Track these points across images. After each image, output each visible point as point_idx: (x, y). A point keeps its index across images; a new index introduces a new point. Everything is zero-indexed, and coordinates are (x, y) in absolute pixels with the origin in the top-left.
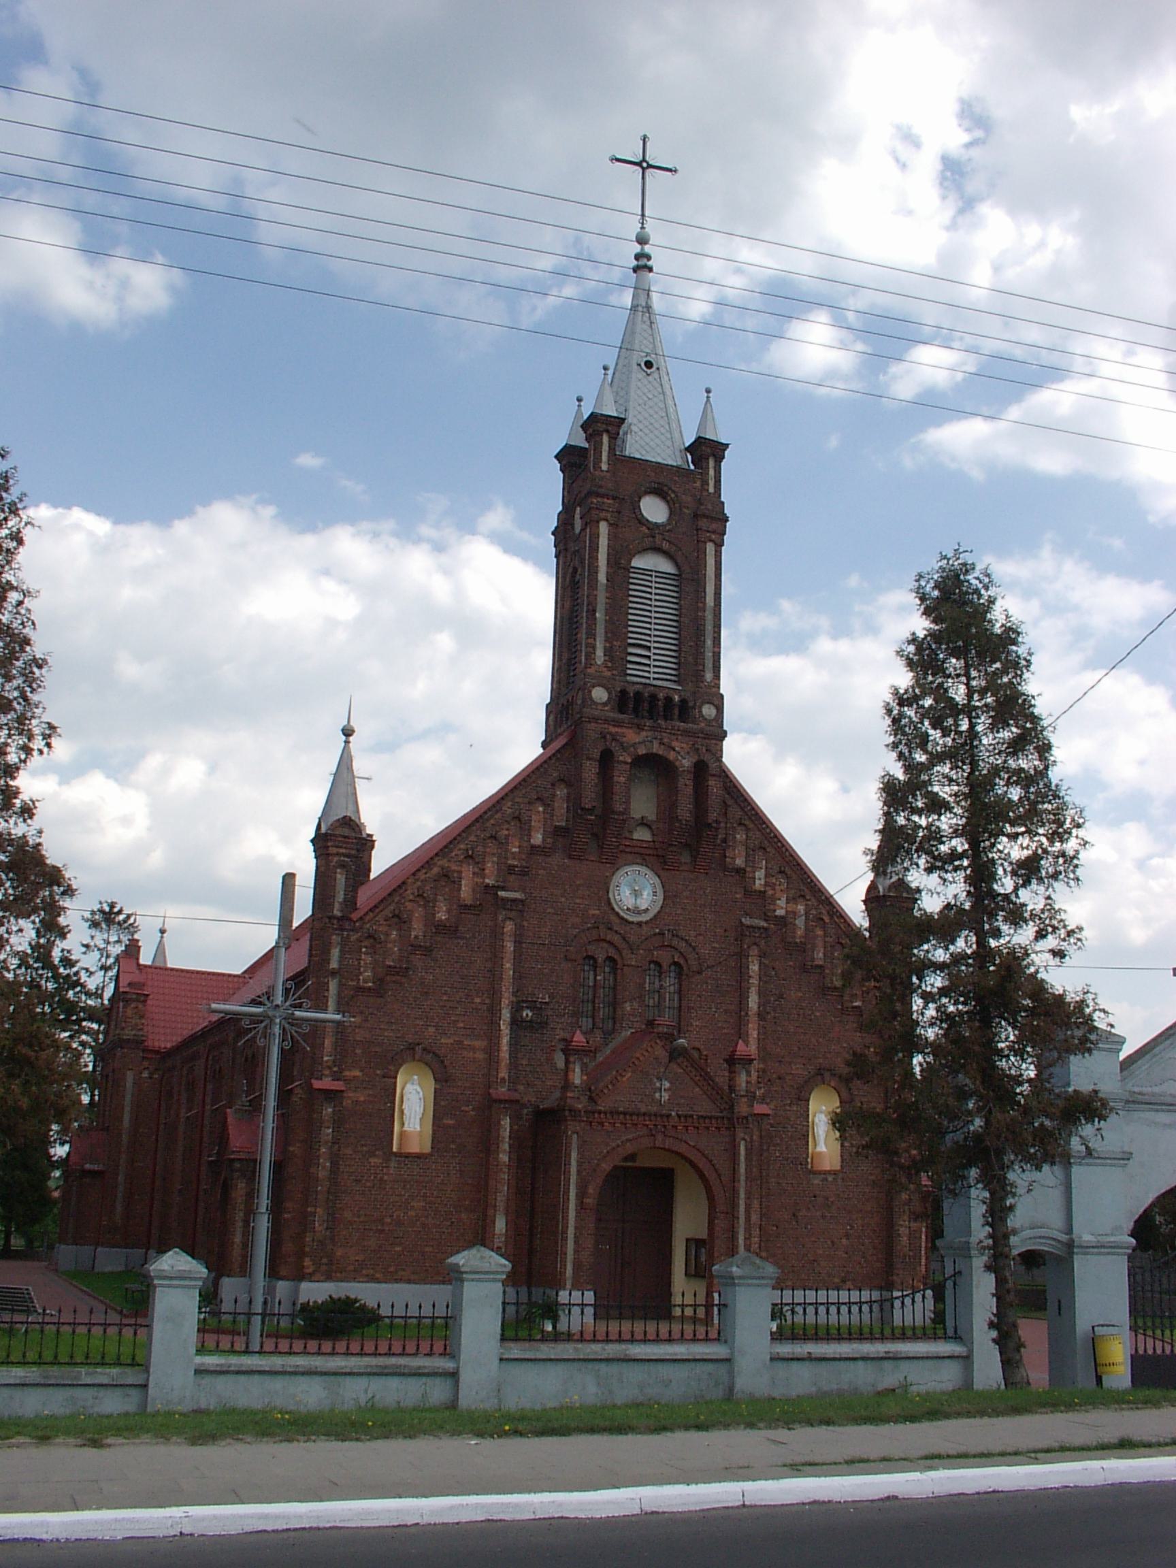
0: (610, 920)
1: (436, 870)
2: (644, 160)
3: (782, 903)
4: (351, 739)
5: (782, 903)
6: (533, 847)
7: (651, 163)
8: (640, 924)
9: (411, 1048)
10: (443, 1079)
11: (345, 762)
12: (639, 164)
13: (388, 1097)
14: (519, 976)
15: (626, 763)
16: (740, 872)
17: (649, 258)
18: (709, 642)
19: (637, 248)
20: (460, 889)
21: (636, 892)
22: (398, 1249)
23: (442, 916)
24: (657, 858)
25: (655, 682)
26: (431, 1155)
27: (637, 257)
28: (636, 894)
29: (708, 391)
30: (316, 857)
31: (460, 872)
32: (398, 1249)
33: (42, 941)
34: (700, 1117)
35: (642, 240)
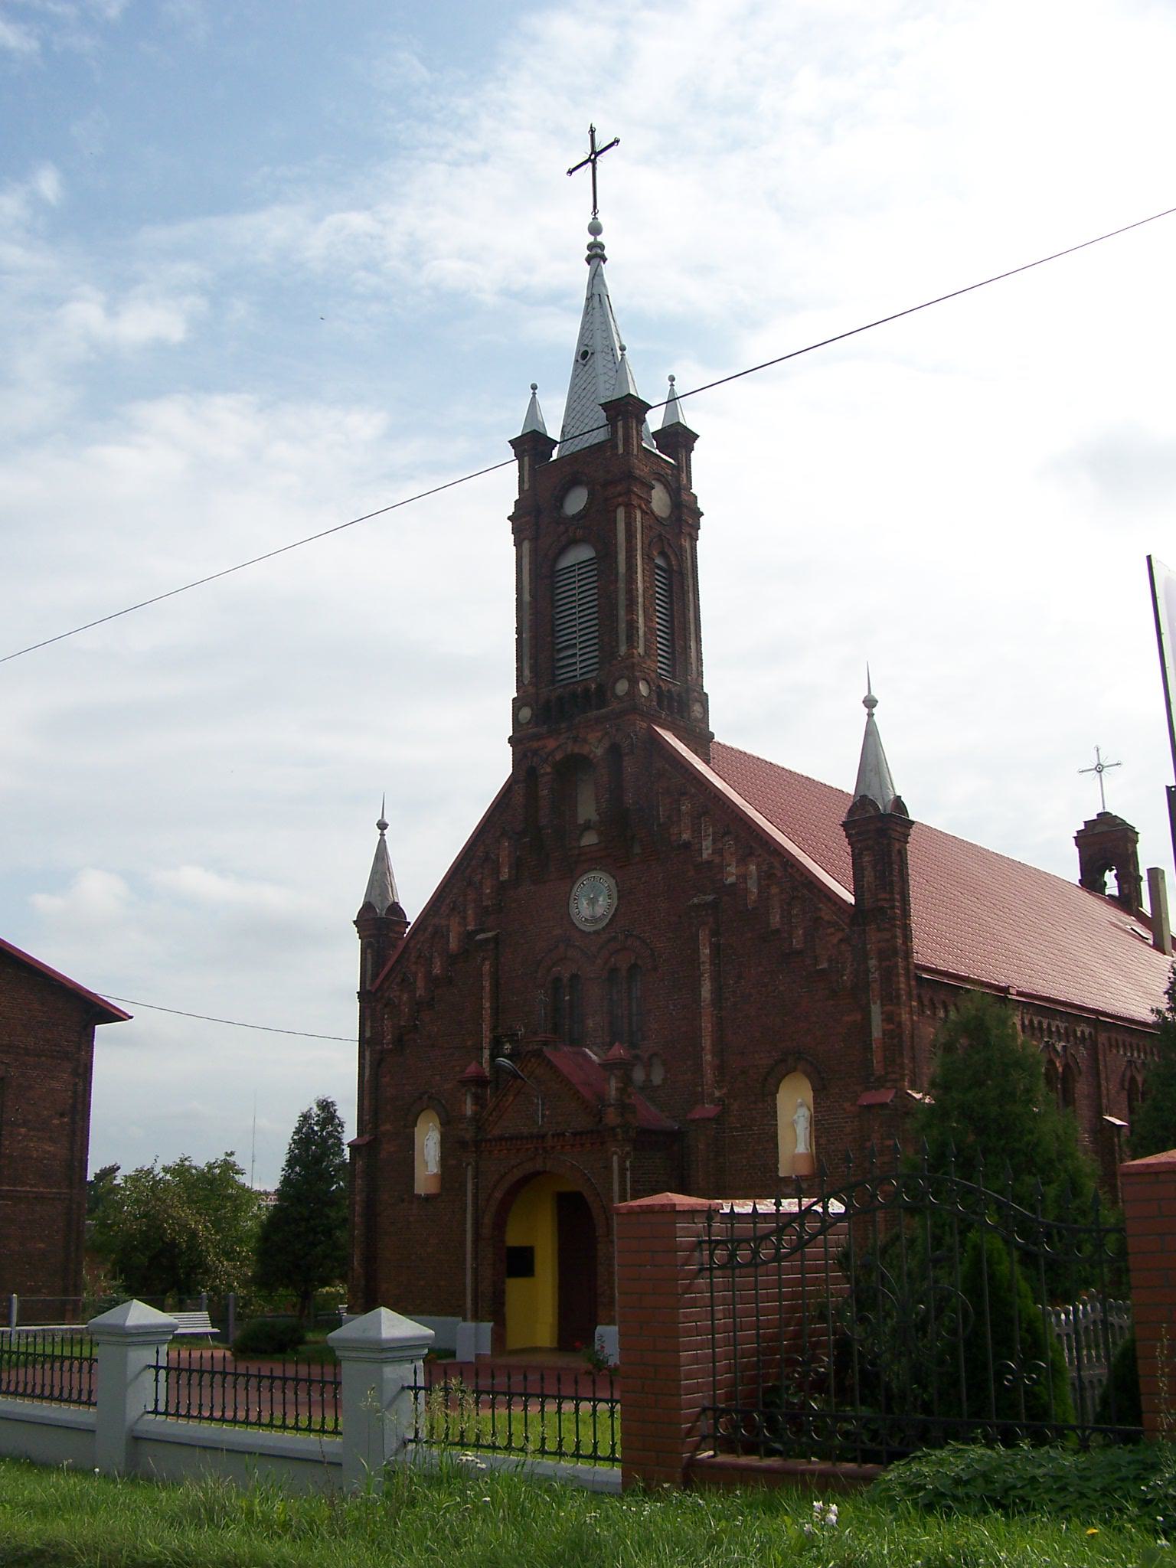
4: (874, 710)
5: (732, 869)
11: (871, 735)
13: (408, 1144)
14: (496, 1011)
17: (601, 246)
19: (591, 239)
22: (422, 1283)
23: (437, 971)
26: (439, 1195)
27: (590, 247)
28: (593, 902)
29: (534, 387)
31: (448, 926)
32: (422, 1283)
35: (595, 229)
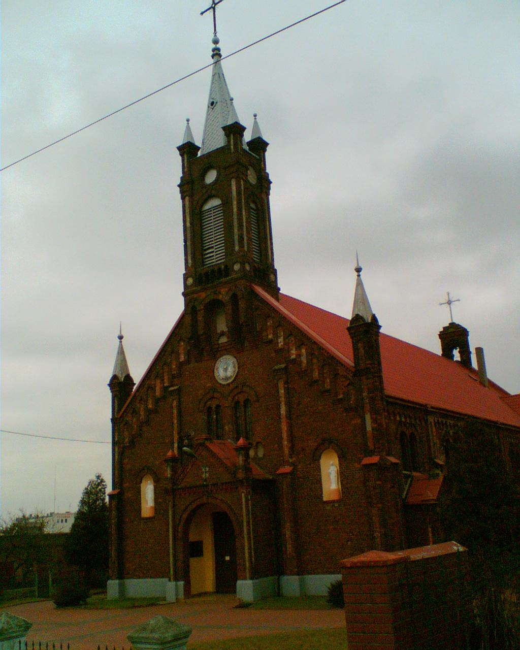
0: (215, 388)
1: (146, 386)
2: (212, 7)
3: (294, 352)
5: (294, 352)
6: (180, 362)
7: (216, 7)
8: (228, 385)
9: (155, 473)
10: (157, 482)
12: (214, 9)
15: (202, 309)
16: (271, 341)
18: (267, 215)
19: (214, 46)
20: (155, 392)
21: (226, 369)
23: (150, 406)
24: (236, 347)
25: (217, 262)
28: (226, 370)
30: (112, 392)
33: (440, 431)
34: (222, 484)
35: (216, 42)
